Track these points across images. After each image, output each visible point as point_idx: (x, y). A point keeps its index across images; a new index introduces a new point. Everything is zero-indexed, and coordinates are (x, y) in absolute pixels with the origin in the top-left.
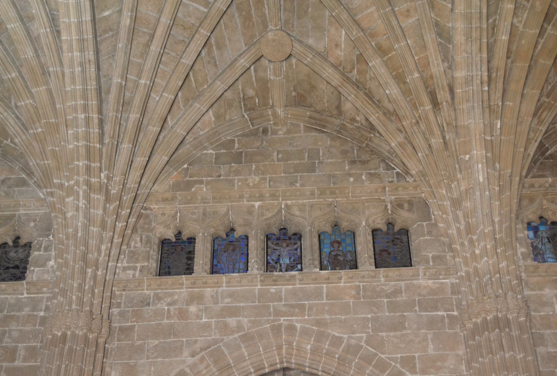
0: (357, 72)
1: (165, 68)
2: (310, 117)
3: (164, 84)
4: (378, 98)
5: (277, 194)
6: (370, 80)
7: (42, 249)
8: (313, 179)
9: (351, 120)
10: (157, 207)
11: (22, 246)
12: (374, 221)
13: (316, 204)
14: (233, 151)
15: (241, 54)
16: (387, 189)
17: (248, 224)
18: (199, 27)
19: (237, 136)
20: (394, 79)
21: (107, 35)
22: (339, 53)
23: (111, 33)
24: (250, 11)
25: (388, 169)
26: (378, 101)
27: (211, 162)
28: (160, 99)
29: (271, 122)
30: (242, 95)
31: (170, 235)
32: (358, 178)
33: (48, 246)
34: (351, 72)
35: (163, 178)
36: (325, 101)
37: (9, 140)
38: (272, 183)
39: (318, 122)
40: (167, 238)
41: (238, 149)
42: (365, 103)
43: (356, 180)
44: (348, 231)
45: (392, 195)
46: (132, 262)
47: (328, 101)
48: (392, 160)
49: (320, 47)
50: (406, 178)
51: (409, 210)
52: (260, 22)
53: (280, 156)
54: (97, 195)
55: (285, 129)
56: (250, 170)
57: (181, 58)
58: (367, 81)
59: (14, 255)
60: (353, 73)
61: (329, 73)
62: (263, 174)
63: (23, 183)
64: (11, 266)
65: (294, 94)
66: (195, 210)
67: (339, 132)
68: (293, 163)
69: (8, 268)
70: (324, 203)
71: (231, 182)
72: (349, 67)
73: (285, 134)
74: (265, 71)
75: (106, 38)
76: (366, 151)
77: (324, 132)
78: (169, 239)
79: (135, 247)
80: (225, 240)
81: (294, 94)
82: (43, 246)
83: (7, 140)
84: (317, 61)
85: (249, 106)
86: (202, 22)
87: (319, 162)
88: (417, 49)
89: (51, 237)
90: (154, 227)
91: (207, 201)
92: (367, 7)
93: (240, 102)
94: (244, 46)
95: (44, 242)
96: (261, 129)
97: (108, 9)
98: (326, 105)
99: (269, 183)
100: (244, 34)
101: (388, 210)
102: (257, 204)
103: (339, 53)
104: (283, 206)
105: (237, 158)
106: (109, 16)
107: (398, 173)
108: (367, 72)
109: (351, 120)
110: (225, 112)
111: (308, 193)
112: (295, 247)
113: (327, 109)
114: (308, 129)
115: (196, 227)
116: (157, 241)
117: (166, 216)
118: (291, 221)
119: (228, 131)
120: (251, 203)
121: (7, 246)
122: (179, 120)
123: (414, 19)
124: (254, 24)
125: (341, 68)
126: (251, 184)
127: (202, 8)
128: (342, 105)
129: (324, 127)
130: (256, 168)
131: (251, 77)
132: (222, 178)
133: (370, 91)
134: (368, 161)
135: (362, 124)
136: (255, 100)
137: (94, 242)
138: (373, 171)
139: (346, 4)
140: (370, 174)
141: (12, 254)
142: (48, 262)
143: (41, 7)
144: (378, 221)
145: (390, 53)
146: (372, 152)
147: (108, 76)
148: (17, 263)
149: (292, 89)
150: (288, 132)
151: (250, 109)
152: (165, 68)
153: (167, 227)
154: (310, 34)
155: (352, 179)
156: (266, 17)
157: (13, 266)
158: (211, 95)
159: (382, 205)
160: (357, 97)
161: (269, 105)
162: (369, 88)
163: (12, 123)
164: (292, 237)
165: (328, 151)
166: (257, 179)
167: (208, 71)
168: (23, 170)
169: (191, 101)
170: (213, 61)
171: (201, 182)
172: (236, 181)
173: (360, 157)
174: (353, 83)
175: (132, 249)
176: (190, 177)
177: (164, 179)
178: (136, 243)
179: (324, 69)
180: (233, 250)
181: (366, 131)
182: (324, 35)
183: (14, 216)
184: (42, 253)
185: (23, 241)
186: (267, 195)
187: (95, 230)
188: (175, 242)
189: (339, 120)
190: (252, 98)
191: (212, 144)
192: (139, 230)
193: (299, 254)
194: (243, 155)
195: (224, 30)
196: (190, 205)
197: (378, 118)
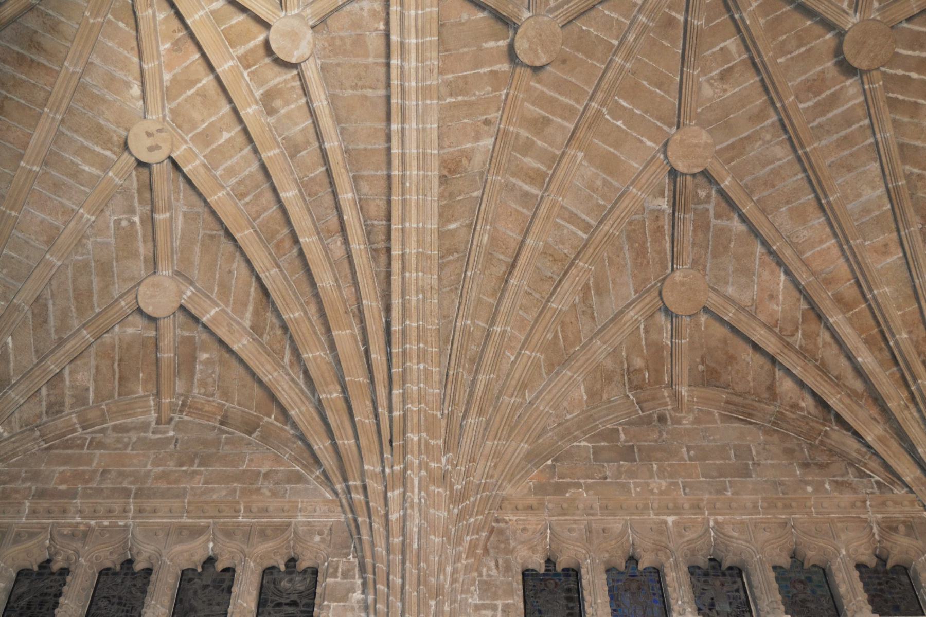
0: (803, 334)
1: (525, 315)
2: (728, 402)
3: (523, 338)
4: (836, 373)
5: (702, 505)
6: (823, 346)
7: (339, 574)
8: (750, 486)
9: (792, 407)
10: (515, 518)
11: (300, 573)
12: (856, 551)
13: (762, 523)
14: (619, 444)
15: (630, 305)
16: (868, 503)
17: (660, 548)
18: (575, 259)
19: (621, 424)
20: (865, 343)
21: (451, 258)
22: (775, 307)
23: (456, 255)
24: (645, 242)
25: (862, 477)
26: (836, 378)
27: (588, 457)
28: (516, 358)
29: (669, 408)
30: (626, 365)
31: (537, 562)
32: (819, 487)
33: (349, 570)
34: (793, 335)
35: (518, 477)
36: (750, 378)
37: (273, 417)
38: (687, 490)
39: (741, 409)
40: (530, 567)
41: (626, 441)
42: (819, 379)
43: (816, 490)
44: (814, 565)
45: (878, 512)
46: (487, 598)
47: (754, 380)
48: (865, 464)
49: (745, 298)
50: (892, 490)
51: (908, 535)
52: (657, 259)
53: (692, 453)
54: (438, 487)
55: (691, 417)
56: (650, 470)
57: (548, 301)
58: (819, 348)
59: (288, 585)
60: (796, 337)
61: (761, 335)
62: (671, 477)
63: (299, 479)
64: (284, 601)
65: (701, 367)
66: (574, 526)
67: (774, 423)
68: (715, 464)
69: (279, 605)
70: (774, 520)
71: (625, 487)
72: (790, 328)
73: (693, 423)
74: (660, 332)
75: (449, 262)
76: (822, 451)
77: (751, 423)
78: (533, 570)
79: (489, 576)
80: (622, 573)
81: (701, 367)
82: (340, 570)
83: (270, 417)
84: (743, 318)
85: (635, 383)
86: (579, 253)
87: (754, 464)
88: (901, 300)
89: (351, 556)
90: (514, 548)
91: (592, 511)
92: (821, 242)
93: (623, 375)
94: (633, 293)
95: (340, 565)
96: (656, 416)
97: (455, 220)
98: (751, 384)
99: (684, 490)
100: (634, 276)
101: (874, 534)
102: (670, 519)
103: (775, 307)
104: (711, 524)
105: (628, 453)
106: (456, 230)
107: (877, 482)
108: (818, 335)
109: (792, 407)
110: (602, 389)
111: (749, 505)
112: (735, 587)
113: (752, 391)
114: (726, 418)
115: (580, 549)
116: (520, 570)
117: (530, 533)
118: (727, 546)
119: (607, 415)
120: (661, 517)
121: (275, 571)
122: (540, 393)
123: (895, 257)
124: (648, 262)
125: (777, 330)
126: (656, 491)
127: (580, 233)
128: (777, 384)
129: (751, 416)
130: (659, 469)
131: (640, 339)
132: (608, 480)
133: (823, 363)
134: (828, 464)
135: (809, 413)
136: (644, 375)
137: (437, 559)
138: (839, 479)
139: (788, 237)
140: (836, 482)
141: (285, 584)
142: (350, 595)
143: (354, 213)
144: (862, 550)
145: (857, 306)
146: (831, 452)
147: (449, 317)
148: (294, 597)
149: (698, 360)
150: (697, 421)
151: (637, 387)
152: (525, 315)
153: (533, 549)
154: (731, 280)
155: (809, 489)
156: (666, 254)
157: (288, 601)
158: (588, 360)
159: (865, 528)
160: (805, 370)
161: (664, 383)
162: (822, 358)
163: (286, 387)
164: (727, 573)
165: (764, 449)
166: (664, 484)
167: (583, 326)
168: (296, 459)
169: (557, 368)
170: (589, 311)
171: (579, 486)
172: (632, 486)
173: (815, 459)
174: (797, 352)
175: (485, 578)
176: (559, 478)
177: (520, 479)
178: (489, 569)
179: (754, 330)
180: (639, 588)
181: (817, 422)
182: (753, 281)
183: (289, 524)
184: (339, 580)
185: (303, 564)
186: (687, 506)
187: (437, 540)
188: (544, 574)
189: (772, 407)
190: (639, 371)
191: (585, 433)
192: (491, 551)
193: (743, 597)
194: (636, 450)
195: (607, 268)
196: (566, 518)
197: (840, 400)
